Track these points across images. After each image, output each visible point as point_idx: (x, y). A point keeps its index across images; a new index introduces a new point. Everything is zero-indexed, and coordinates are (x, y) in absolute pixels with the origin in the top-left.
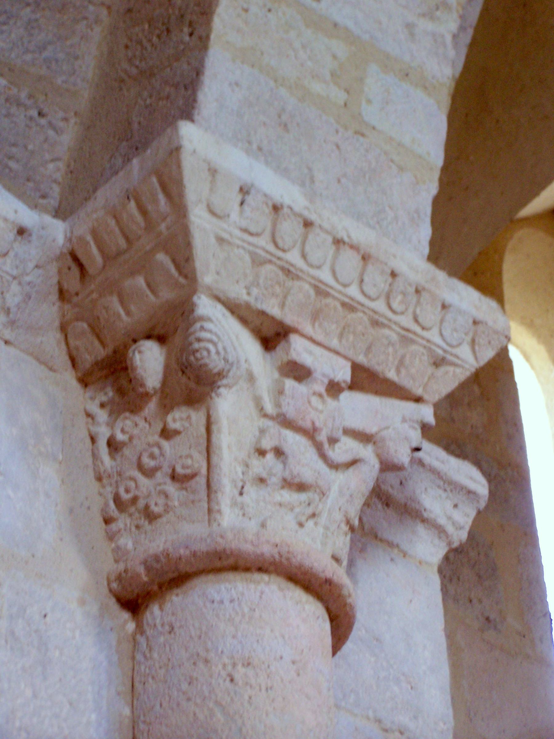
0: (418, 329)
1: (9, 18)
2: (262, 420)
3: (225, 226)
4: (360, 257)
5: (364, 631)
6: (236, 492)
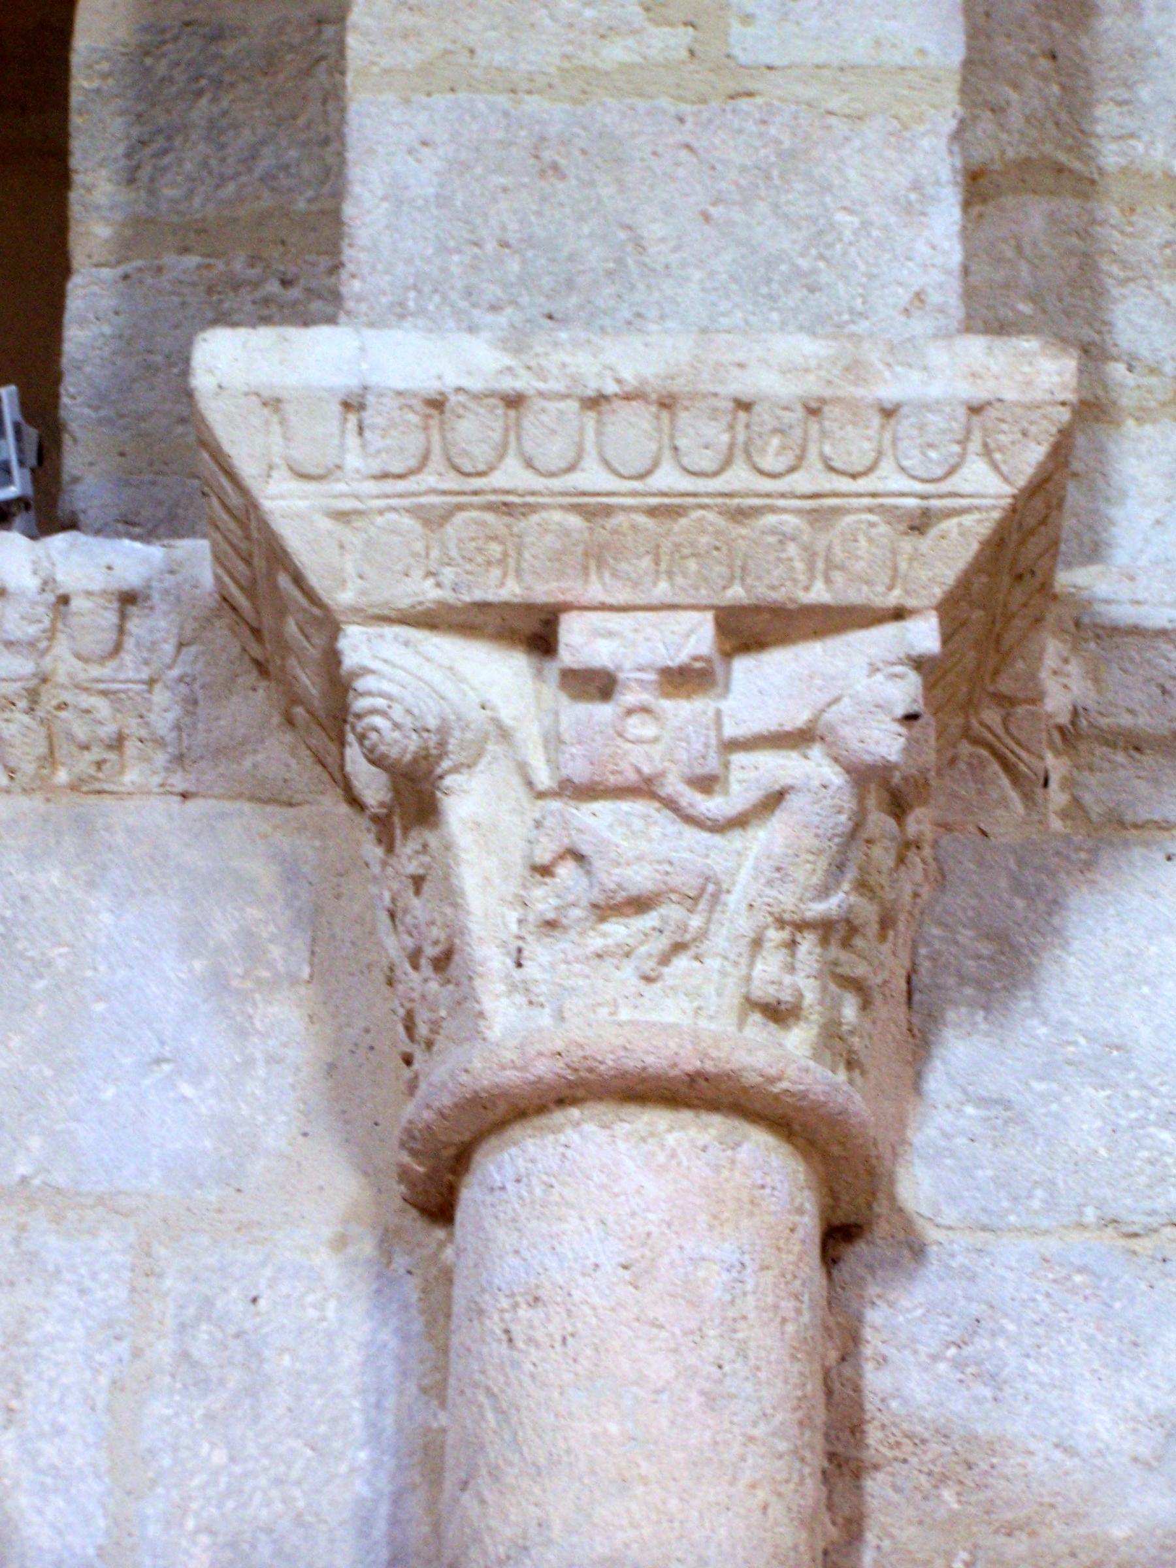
1: (169, 138)
2: (540, 803)
3: (341, 487)
6: (510, 963)
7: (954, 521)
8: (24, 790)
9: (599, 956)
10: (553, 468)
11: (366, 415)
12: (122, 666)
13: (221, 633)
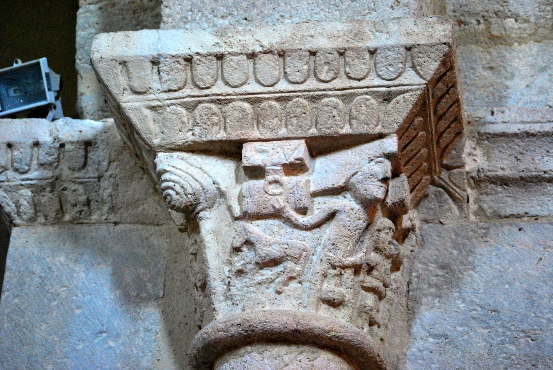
0: (355, 84)
3: (152, 96)
4: (276, 57)
5: (479, 309)
7: (402, 96)
8: (51, 224)
9: (259, 284)
10: (236, 84)
11: (160, 66)
12: (87, 171)
13: (126, 156)
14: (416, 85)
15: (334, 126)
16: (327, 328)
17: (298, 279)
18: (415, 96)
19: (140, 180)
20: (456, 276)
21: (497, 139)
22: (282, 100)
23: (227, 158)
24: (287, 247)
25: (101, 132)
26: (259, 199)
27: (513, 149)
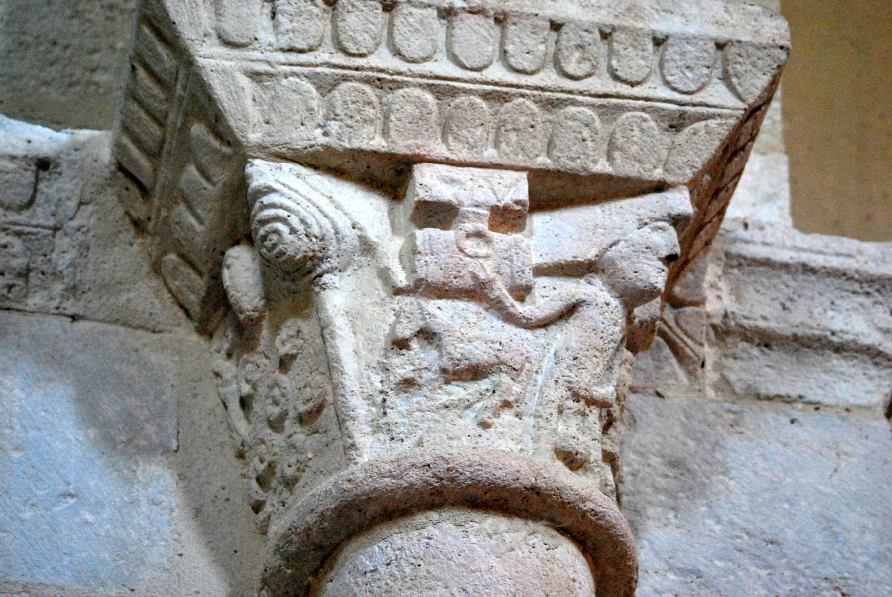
0: (625, 89)
3: (256, 55)
4: (492, 22)
5: (746, 537)
7: (703, 123)
9: (446, 407)
10: (416, 56)
14: (729, 108)
15: (582, 157)
16: (583, 493)
17: (515, 409)
18: (725, 127)
19: (128, 247)
20: (698, 479)
21: (756, 269)
22: (493, 98)
23: (373, 191)
24: (500, 348)
25: (69, 148)
26: (448, 260)
27: (779, 290)
